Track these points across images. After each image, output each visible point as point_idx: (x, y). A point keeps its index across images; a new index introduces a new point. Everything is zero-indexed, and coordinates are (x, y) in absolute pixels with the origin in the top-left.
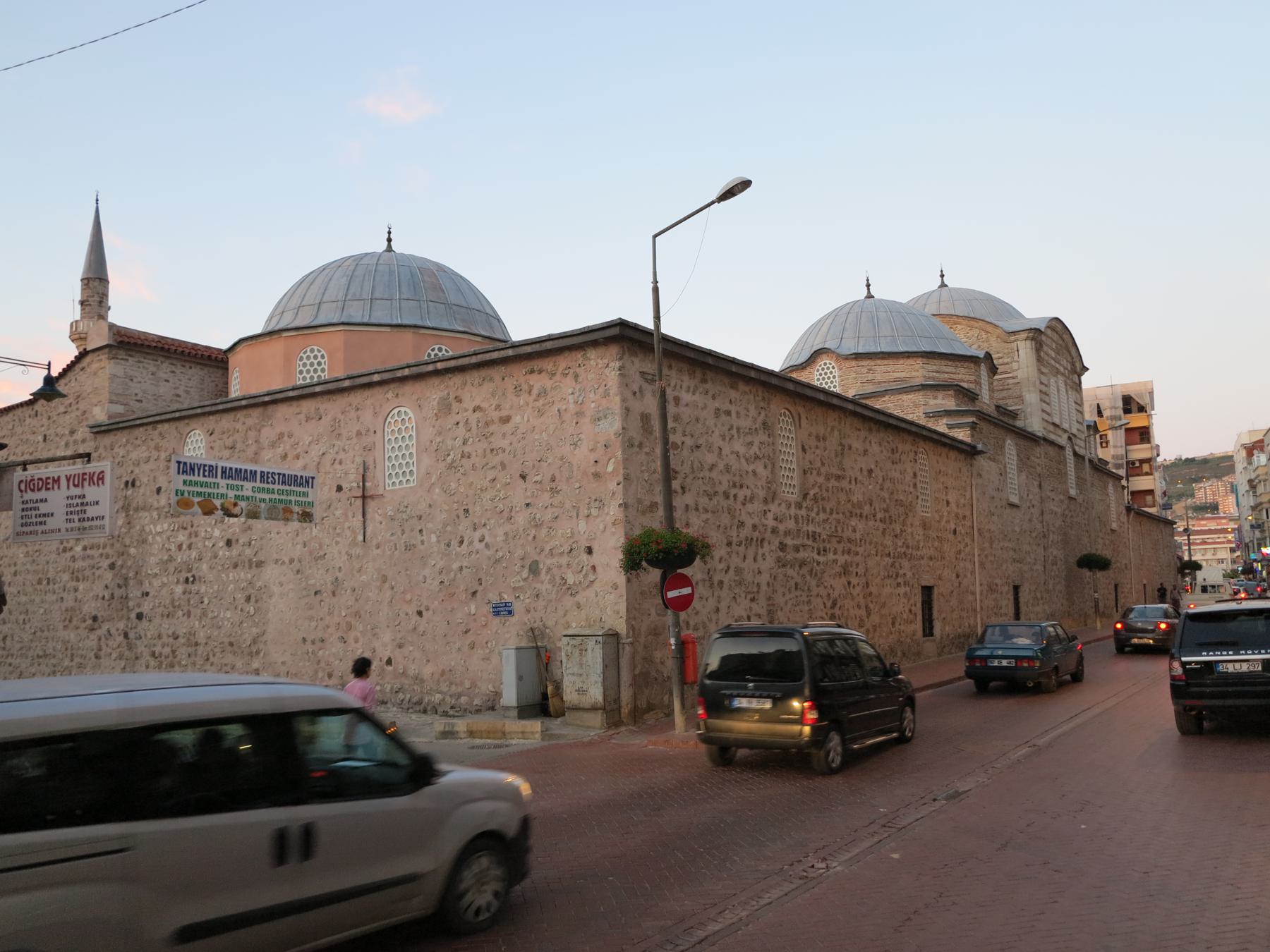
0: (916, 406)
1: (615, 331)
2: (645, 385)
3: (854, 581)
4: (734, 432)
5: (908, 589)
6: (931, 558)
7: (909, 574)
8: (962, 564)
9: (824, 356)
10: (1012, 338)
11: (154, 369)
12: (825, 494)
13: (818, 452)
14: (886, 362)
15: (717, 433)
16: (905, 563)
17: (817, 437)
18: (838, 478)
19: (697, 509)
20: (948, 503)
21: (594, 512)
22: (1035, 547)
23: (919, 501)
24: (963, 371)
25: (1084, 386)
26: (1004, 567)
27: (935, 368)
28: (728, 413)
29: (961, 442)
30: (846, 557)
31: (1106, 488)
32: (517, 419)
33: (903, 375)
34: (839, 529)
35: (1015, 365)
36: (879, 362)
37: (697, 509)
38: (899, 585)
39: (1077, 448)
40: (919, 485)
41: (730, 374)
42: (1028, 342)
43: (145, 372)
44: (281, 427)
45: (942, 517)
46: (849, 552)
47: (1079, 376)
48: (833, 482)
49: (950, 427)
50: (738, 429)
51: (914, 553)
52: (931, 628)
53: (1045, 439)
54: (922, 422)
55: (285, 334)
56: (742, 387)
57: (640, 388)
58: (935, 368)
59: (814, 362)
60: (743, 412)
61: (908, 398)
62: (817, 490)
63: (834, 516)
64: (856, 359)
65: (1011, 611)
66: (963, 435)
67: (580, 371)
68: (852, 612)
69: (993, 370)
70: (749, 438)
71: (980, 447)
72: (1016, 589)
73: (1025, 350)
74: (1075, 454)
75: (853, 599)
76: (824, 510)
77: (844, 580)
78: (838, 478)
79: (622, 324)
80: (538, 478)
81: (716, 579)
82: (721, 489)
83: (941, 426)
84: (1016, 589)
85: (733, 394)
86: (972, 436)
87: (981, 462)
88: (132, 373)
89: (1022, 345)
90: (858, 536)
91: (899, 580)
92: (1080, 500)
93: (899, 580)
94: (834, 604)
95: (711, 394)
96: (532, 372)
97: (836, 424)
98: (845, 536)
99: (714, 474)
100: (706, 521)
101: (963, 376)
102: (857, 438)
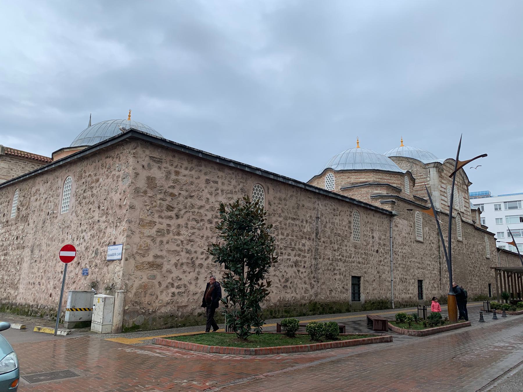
0: (367, 193)
1: (129, 135)
2: (152, 163)
3: (302, 270)
4: (219, 191)
5: (342, 277)
6: (359, 263)
7: (343, 269)
8: (381, 267)
9: (329, 172)
10: (427, 167)
11: (24, 166)
12: (284, 226)
13: (280, 206)
14: (356, 174)
15: (206, 191)
16: (340, 264)
17: (280, 199)
18: (294, 219)
19: (187, 227)
20: (373, 237)
21: (118, 224)
22: (433, 263)
23: (352, 235)
24: (395, 179)
25: (470, 191)
26: (412, 270)
27: (380, 177)
28: (216, 182)
29: (387, 211)
30: (297, 258)
31: (483, 238)
32: (101, 180)
33: (364, 180)
34: (293, 244)
35: (428, 179)
36: (353, 174)
37: (187, 227)
38: (335, 274)
39: (464, 219)
40: (352, 227)
41: (189, 155)
42: (435, 169)
43: (19, 167)
44: (37, 187)
45: (368, 244)
46: (299, 255)
47: (467, 186)
48: (290, 221)
49: (382, 203)
50: (222, 191)
51: (347, 259)
52: (422, 296)
53: (442, 213)
54: (341, 193)
55: (65, 150)
56: (227, 171)
57: (149, 164)
58: (380, 177)
59: (325, 174)
60: (226, 182)
61: (364, 190)
62: (278, 223)
63: (290, 237)
64: (342, 173)
65: (416, 292)
66: (388, 207)
67: (121, 155)
68: (300, 286)
69: (413, 180)
70: (230, 195)
71: (394, 212)
72: (420, 282)
73: (433, 172)
74: (463, 221)
75: (301, 279)
76: (283, 234)
77: (295, 269)
78: (294, 219)
79: (132, 131)
80: (103, 208)
81: (197, 262)
82: (206, 218)
83: (377, 204)
84: (420, 282)
85: (220, 174)
86: (392, 207)
87: (396, 219)
88: (12, 167)
89: (431, 170)
90: (307, 248)
91: (336, 272)
92: (465, 242)
93: (336, 272)
94: (287, 280)
95: (203, 172)
96: (107, 157)
97: (295, 194)
98: (297, 247)
99: (202, 211)
100: (193, 234)
101: (395, 182)
102: (308, 202)
